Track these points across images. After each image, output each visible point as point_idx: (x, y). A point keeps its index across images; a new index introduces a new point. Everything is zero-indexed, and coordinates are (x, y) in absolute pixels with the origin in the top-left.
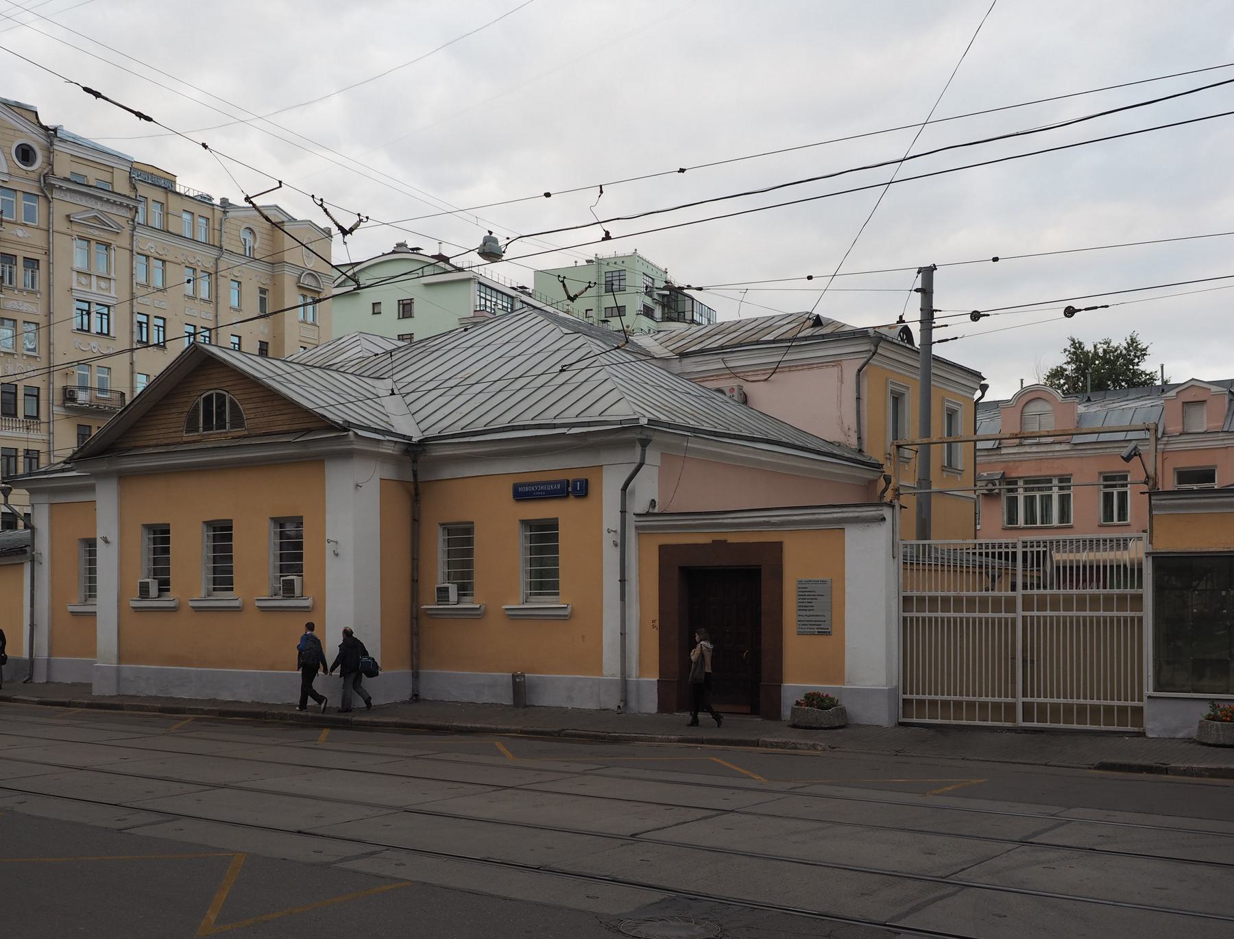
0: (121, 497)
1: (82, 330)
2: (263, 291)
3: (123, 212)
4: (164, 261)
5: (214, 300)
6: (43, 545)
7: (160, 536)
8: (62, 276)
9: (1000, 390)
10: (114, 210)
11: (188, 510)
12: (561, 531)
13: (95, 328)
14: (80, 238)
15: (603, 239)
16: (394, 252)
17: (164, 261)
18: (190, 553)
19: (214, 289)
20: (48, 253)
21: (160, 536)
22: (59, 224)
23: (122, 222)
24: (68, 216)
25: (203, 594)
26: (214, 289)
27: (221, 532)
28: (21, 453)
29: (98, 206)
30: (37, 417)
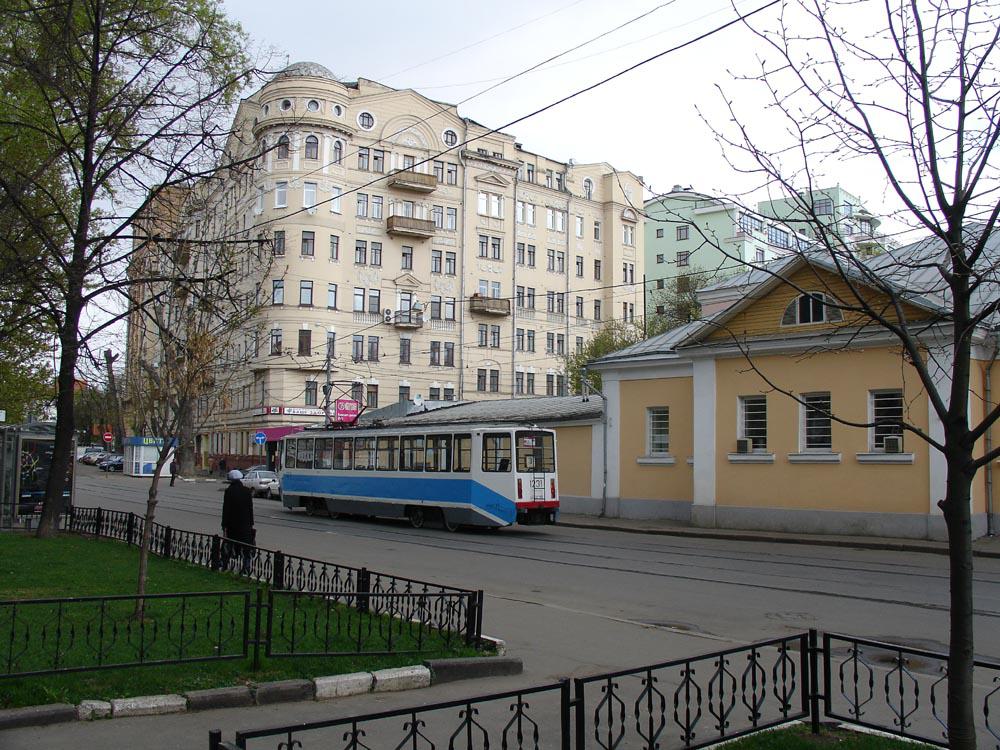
0: (717, 367)
1: (482, 256)
2: (596, 224)
3: (509, 172)
4: (534, 205)
5: (567, 231)
6: (614, 413)
7: (756, 410)
8: (472, 221)
9: (101, 388)
10: (505, 170)
11: (788, 387)
12: (768, 404)
13: (490, 255)
14: (483, 192)
15: (329, 308)
16: (673, 192)
17: (534, 205)
18: (789, 423)
19: (566, 224)
20: (462, 204)
21: (756, 410)
22: (470, 183)
23: (509, 179)
24: (475, 178)
25: (647, 453)
26: (566, 224)
27: (819, 408)
28: (526, 332)
29: (495, 169)
30: (453, 320)
